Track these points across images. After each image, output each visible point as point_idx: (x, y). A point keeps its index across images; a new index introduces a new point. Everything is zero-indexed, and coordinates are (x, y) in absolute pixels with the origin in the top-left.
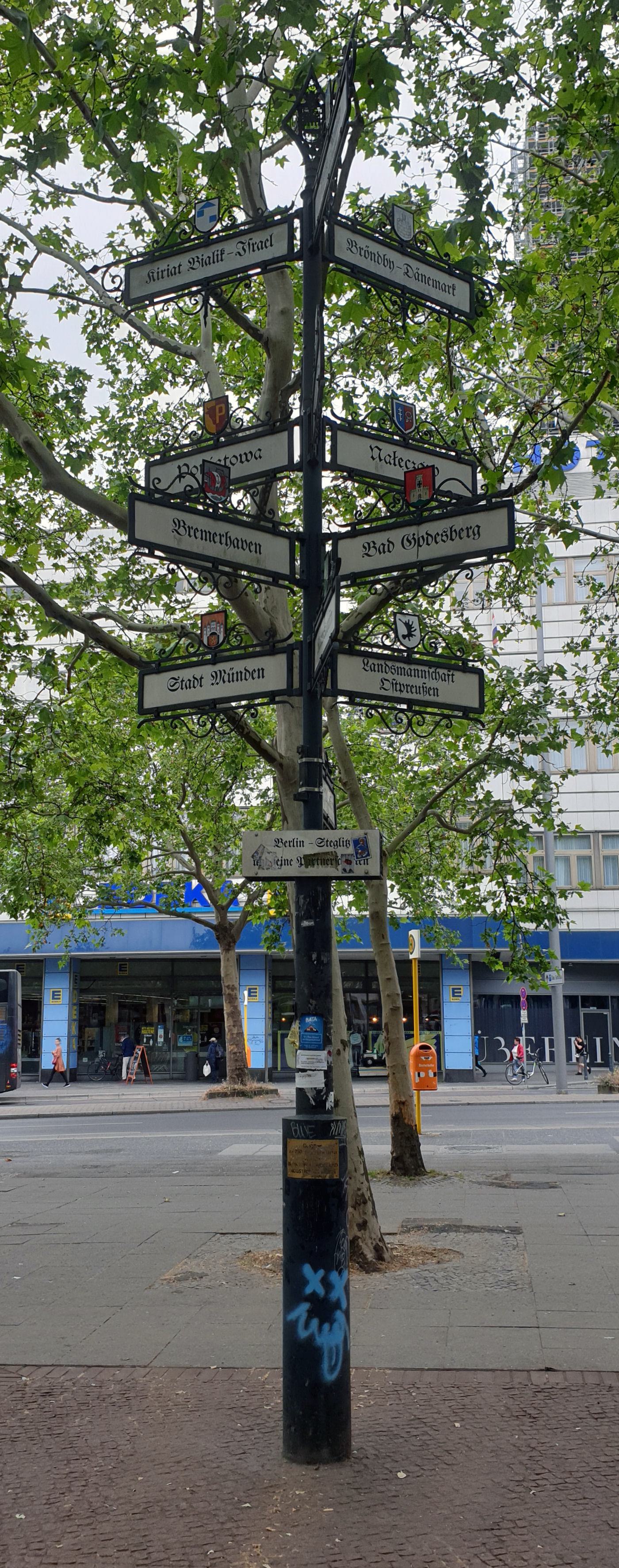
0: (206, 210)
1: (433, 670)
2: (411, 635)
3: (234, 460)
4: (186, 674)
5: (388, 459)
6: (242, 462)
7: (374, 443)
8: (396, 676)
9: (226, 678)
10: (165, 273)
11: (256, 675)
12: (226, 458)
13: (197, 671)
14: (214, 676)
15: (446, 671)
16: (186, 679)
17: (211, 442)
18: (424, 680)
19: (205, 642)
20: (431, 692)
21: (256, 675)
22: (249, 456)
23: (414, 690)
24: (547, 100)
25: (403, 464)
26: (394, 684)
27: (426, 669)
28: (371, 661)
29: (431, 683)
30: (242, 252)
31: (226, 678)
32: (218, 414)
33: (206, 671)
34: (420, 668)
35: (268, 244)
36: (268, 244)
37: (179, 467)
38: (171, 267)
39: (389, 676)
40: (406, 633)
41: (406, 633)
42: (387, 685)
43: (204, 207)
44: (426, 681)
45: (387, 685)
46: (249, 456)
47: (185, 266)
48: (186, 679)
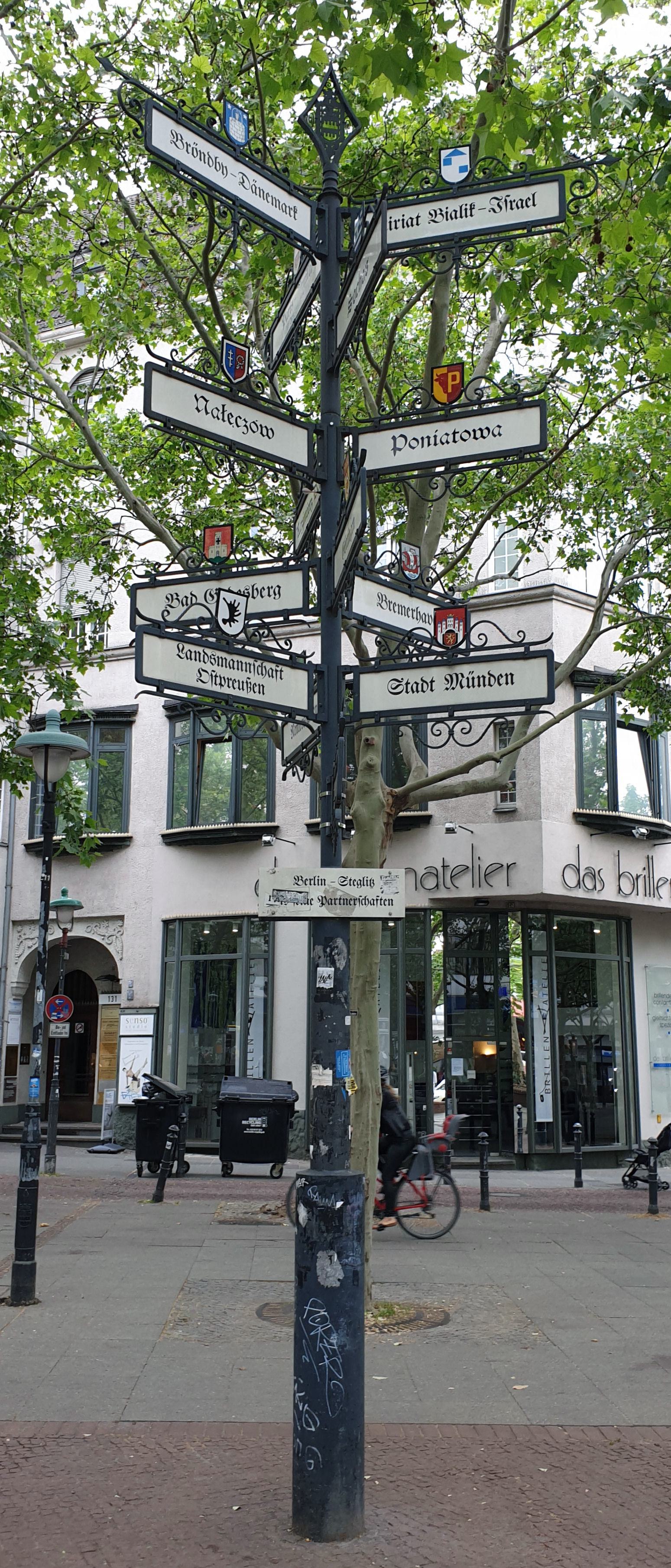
0: (454, 158)
1: (259, 663)
2: (234, 621)
3: (465, 436)
4: (413, 676)
5: (215, 413)
6: (475, 438)
7: (200, 392)
8: (215, 667)
9: (465, 683)
10: (399, 224)
11: (503, 680)
12: (454, 433)
13: (428, 674)
14: (449, 679)
15: (273, 666)
16: (412, 682)
17: (442, 413)
18: (248, 674)
19: (440, 640)
20: (256, 689)
21: (503, 680)
22: (485, 433)
23: (236, 685)
24: (515, 36)
25: (233, 420)
26: (214, 677)
27: (251, 661)
28: (188, 647)
29: (256, 679)
30: (498, 209)
31: (465, 683)
32: (450, 383)
33: (438, 674)
34: (245, 660)
35: (530, 203)
36: (530, 203)
37: (394, 438)
38: (406, 218)
39: (208, 667)
40: (227, 617)
41: (227, 617)
42: (205, 677)
43: (451, 155)
44: (251, 675)
45: (205, 677)
46: (485, 433)
47: (425, 218)
48: (412, 682)
